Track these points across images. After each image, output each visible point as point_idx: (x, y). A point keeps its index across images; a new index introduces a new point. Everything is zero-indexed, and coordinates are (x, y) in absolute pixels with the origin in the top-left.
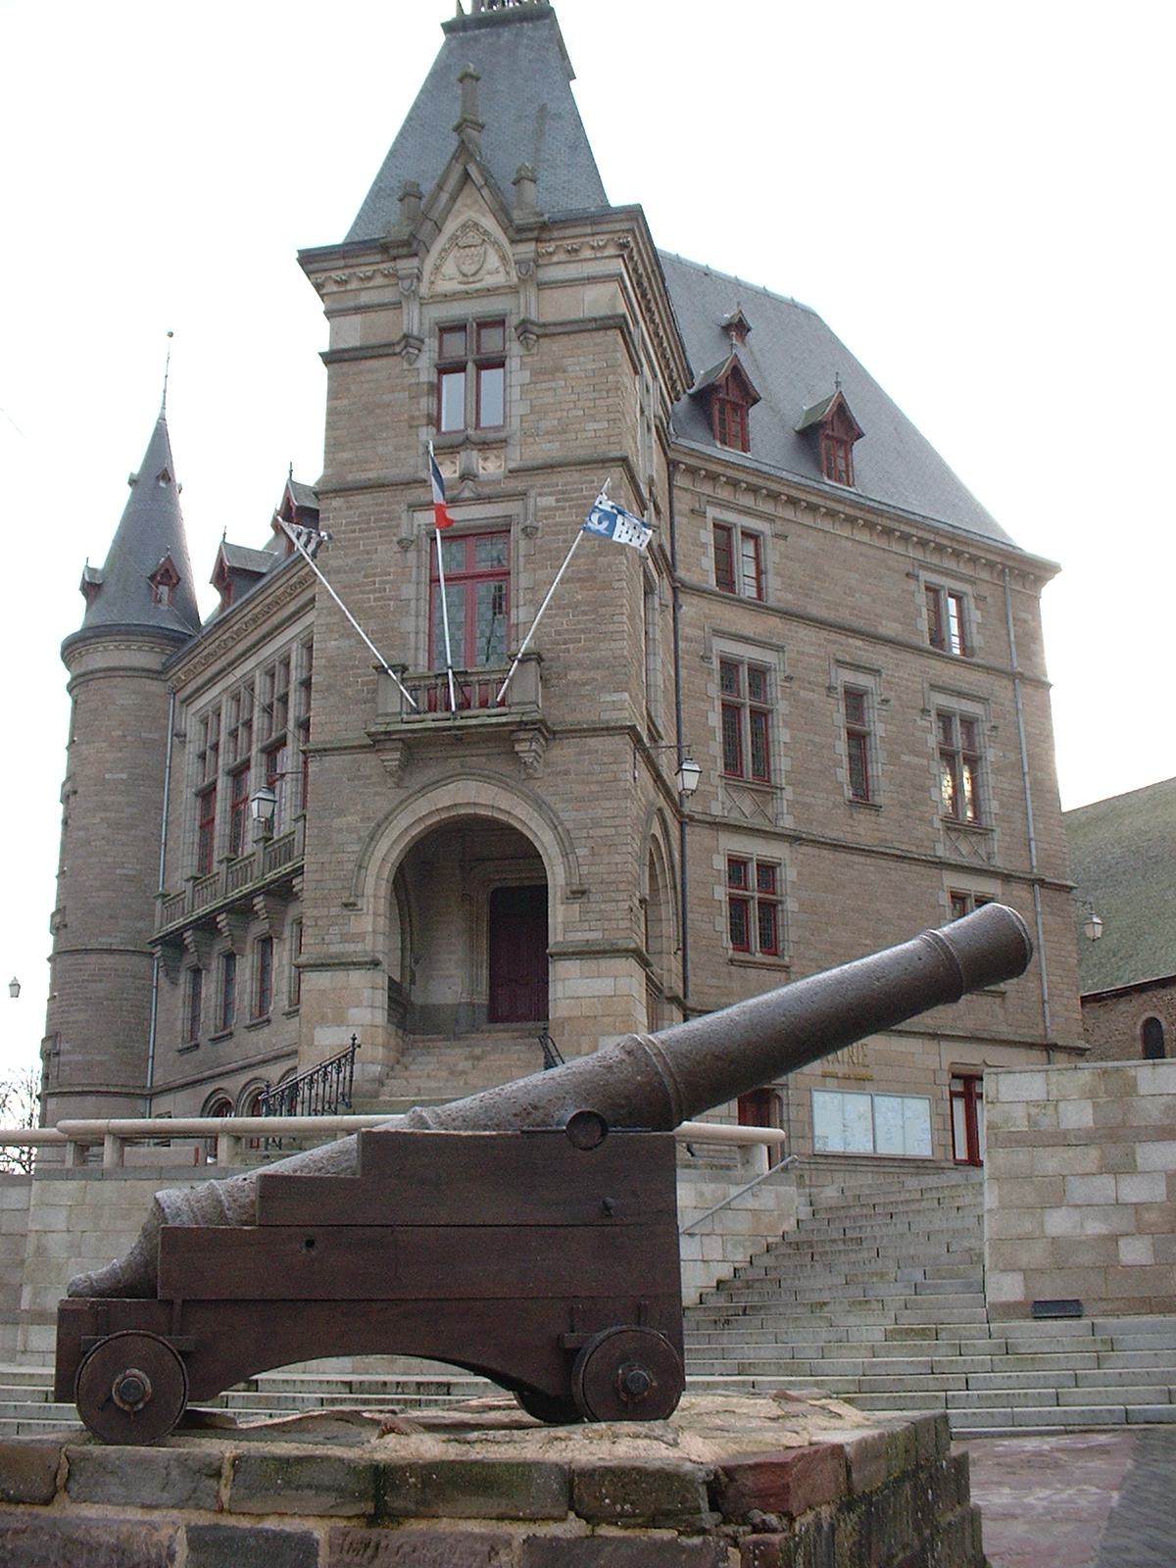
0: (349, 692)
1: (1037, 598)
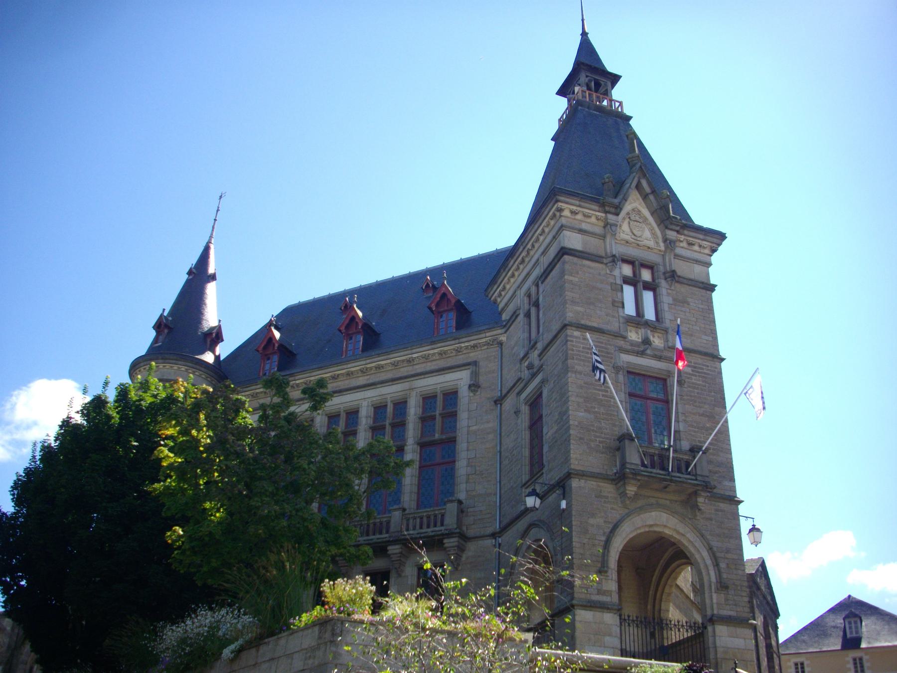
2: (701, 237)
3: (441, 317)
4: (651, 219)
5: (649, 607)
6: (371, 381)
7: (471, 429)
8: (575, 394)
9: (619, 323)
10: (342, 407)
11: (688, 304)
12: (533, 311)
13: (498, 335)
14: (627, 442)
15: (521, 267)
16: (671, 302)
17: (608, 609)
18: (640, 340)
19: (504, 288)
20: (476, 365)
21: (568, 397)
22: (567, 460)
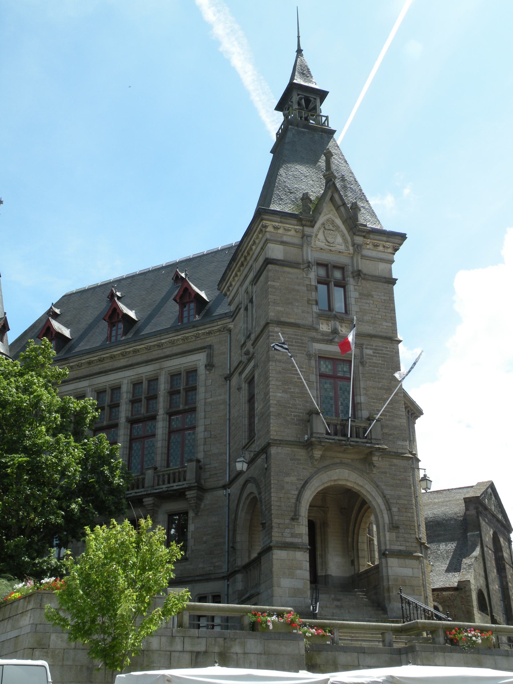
0: (288, 418)
1: (415, 423)
2: (384, 239)
3: (185, 307)
4: (342, 227)
5: (350, 540)
6: (130, 363)
7: (208, 400)
8: (275, 379)
9: (313, 318)
10: (107, 384)
11: (372, 297)
12: (250, 305)
13: (228, 323)
14: (314, 416)
15: (242, 269)
16: (357, 296)
17: (299, 548)
18: (330, 331)
19: (231, 285)
20: (210, 349)
21: (269, 382)
22: (268, 432)
